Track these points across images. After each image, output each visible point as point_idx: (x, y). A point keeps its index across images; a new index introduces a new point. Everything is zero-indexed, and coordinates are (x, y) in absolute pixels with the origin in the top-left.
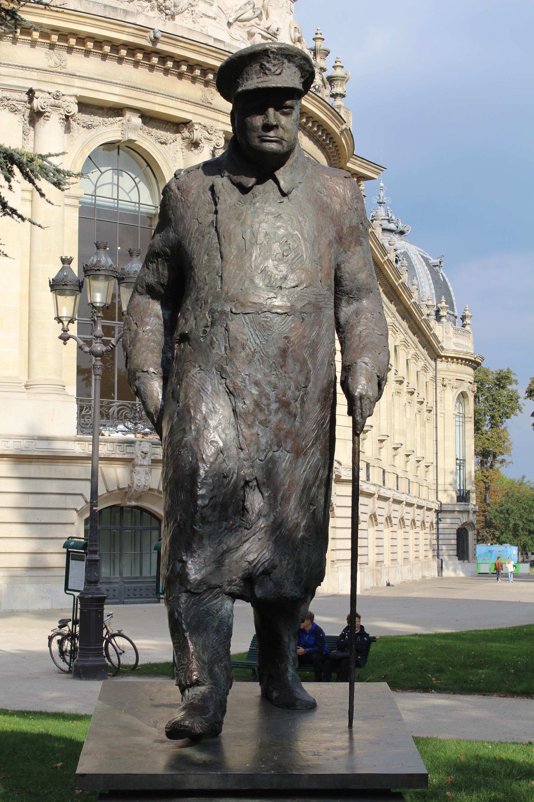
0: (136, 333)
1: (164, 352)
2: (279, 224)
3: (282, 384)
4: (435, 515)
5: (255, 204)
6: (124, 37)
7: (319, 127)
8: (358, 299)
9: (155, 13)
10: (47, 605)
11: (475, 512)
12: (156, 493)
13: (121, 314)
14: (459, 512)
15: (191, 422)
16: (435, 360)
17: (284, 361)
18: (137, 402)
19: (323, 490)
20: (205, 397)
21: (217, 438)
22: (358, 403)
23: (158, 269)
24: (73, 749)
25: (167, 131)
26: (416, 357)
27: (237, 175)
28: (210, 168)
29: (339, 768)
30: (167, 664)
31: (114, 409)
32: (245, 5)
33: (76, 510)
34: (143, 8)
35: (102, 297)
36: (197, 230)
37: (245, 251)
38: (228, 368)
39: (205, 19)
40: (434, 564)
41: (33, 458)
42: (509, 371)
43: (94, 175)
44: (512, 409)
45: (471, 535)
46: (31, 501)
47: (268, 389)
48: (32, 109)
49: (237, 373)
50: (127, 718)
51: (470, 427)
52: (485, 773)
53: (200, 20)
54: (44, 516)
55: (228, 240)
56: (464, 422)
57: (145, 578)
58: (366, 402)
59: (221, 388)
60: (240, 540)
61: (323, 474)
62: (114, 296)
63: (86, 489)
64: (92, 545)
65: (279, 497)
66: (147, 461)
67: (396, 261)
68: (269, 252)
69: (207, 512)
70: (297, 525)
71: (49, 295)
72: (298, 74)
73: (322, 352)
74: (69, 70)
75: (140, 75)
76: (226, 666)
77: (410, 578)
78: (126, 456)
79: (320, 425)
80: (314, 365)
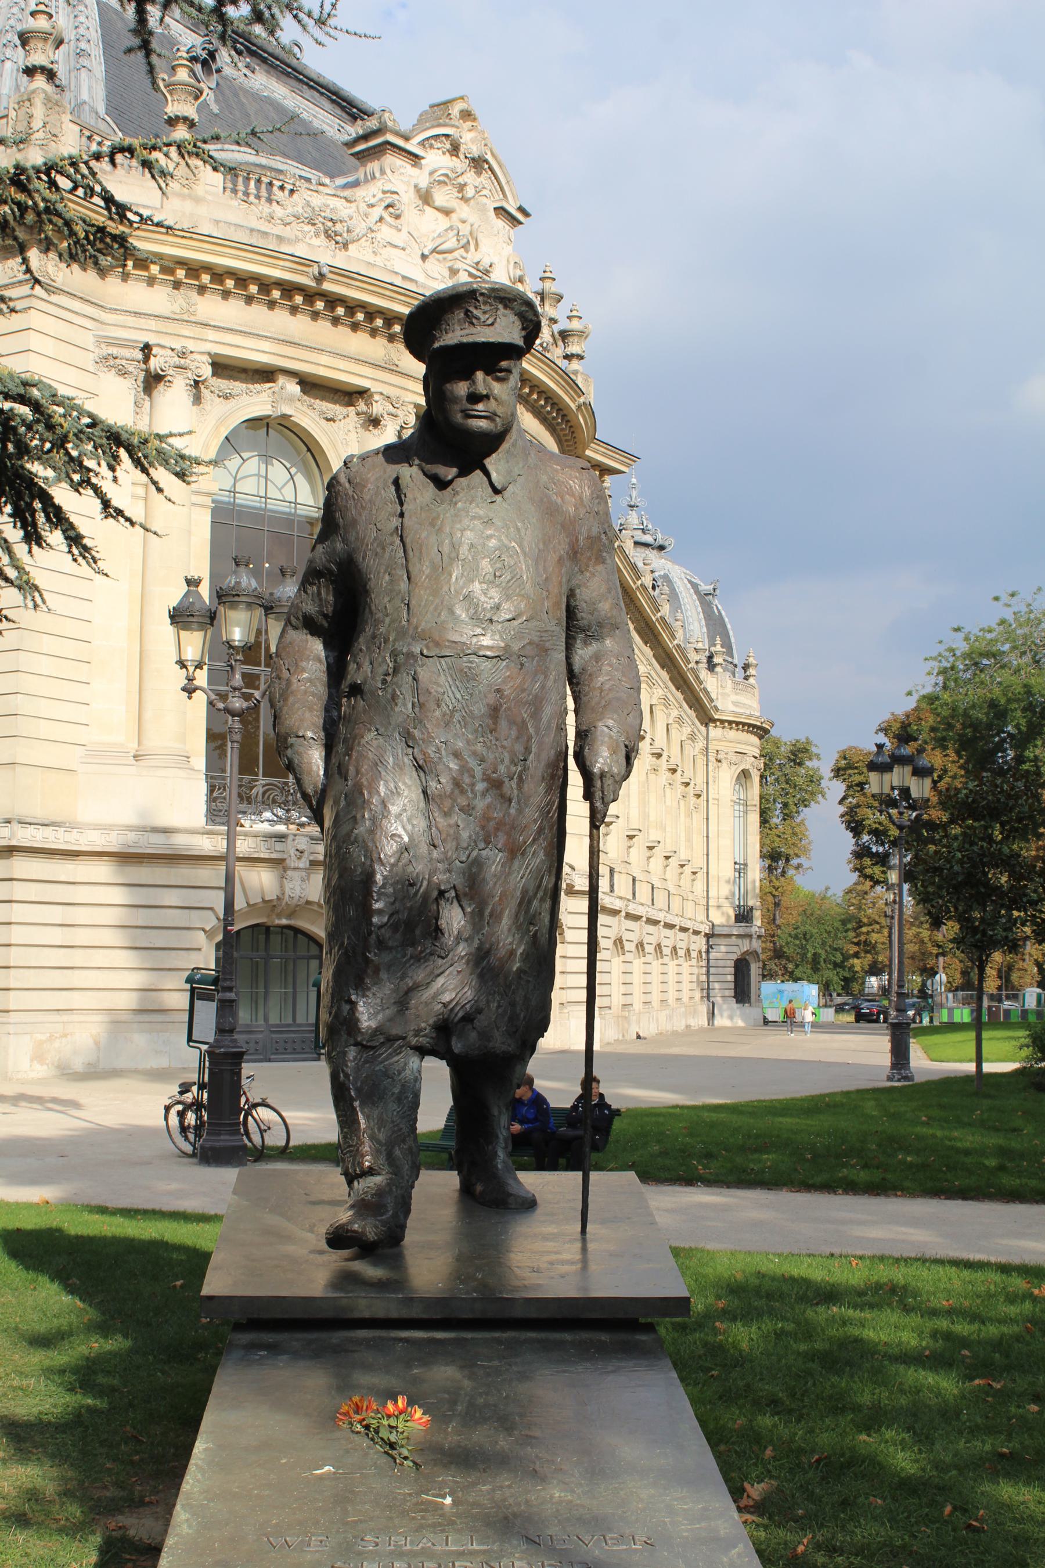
0: (289, 682)
1: (327, 710)
2: (489, 532)
4: (704, 940)
5: (456, 504)
6: (277, 274)
8: (599, 638)
11: (759, 937)
12: (315, 908)
13: (269, 656)
14: (739, 936)
15: (364, 808)
16: (706, 725)
19: (547, 905)
20: (383, 773)
22: (598, 784)
23: (319, 593)
25: (335, 403)
26: (680, 720)
28: (394, 453)
31: (258, 790)
32: (446, 230)
33: (203, 930)
35: (242, 634)
36: (375, 539)
37: (441, 569)
39: (389, 249)
40: (703, 1009)
41: (144, 858)
42: (808, 742)
44: (813, 794)
45: (755, 969)
46: (142, 917)
47: (472, 763)
48: (147, 371)
49: (429, 740)
50: (273, 1220)
51: (754, 818)
52: (769, 1296)
53: (384, 251)
55: (417, 554)
56: (746, 812)
57: (300, 1025)
58: (608, 781)
59: (406, 760)
60: (432, 972)
61: (548, 882)
62: (259, 632)
64: (225, 980)
65: (487, 913)
66: (303, 863)
67: (654, 588)
68: (475, 572)
69: (386, 933)
71: (169, 630)
72: (518, 324)
73: (548, 711)
74: (200, 317)
75: (299, 326)
76: (410, 1149)
77: (669, 1028)
78: (274, 856)
79: (545, 814)
80: (537, 729)
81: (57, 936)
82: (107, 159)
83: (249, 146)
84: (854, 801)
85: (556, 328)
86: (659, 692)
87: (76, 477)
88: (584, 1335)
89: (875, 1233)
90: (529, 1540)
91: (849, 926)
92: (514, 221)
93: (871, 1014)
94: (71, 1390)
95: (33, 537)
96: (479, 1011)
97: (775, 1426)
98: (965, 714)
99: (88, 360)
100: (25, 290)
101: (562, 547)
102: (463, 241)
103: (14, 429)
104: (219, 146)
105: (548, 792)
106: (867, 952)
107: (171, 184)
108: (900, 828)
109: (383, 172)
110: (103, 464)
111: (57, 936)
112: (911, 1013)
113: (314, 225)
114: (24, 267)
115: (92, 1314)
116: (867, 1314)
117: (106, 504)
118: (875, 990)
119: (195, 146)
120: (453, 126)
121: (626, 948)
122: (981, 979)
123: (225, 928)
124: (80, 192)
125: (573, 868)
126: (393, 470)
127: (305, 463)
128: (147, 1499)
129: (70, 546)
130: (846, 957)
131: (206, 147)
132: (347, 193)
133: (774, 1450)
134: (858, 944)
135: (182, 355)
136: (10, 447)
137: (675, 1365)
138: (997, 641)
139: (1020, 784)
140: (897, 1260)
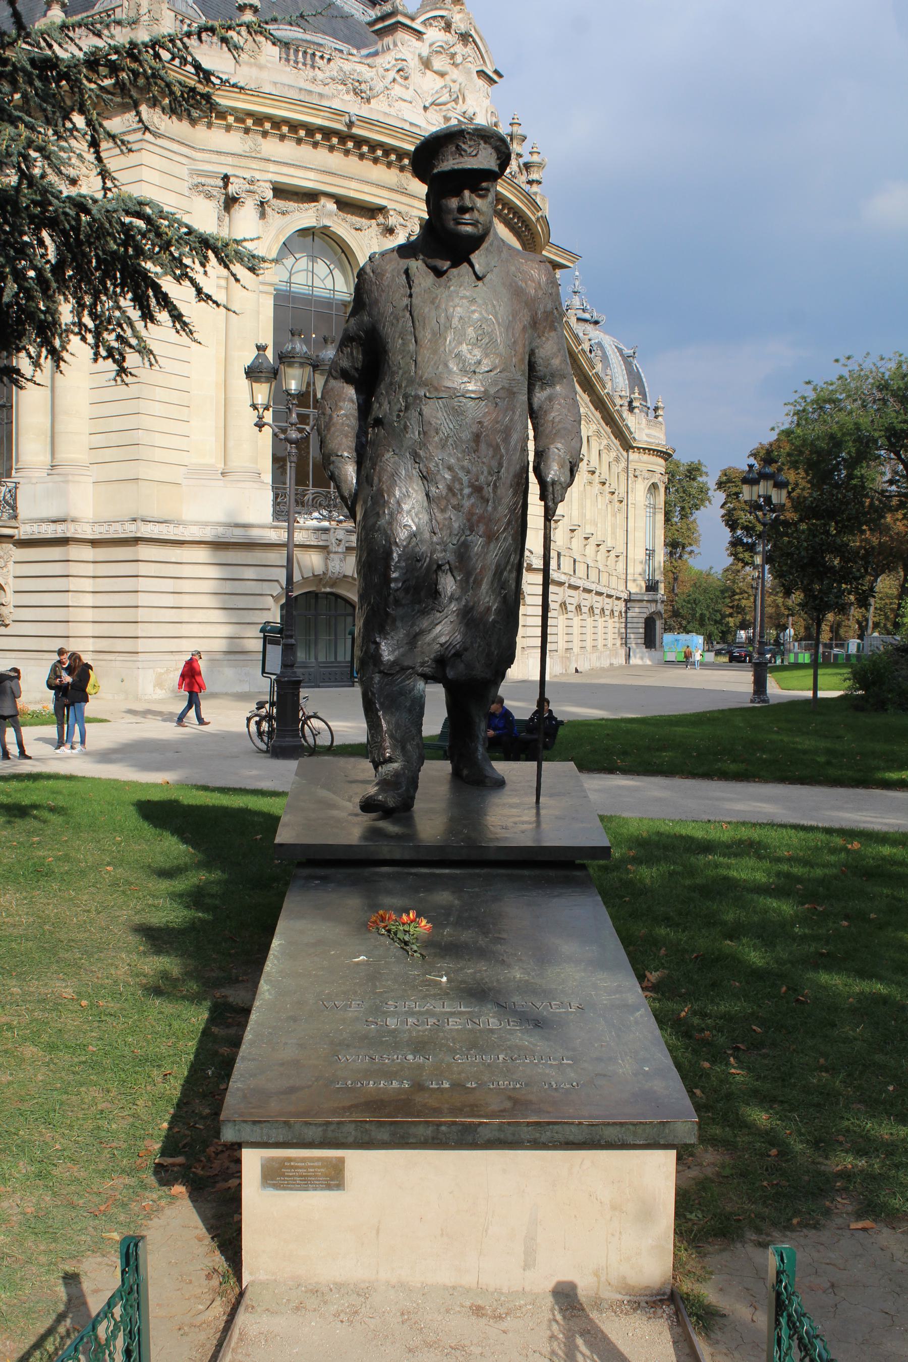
0: (331, 417)
1: (358, 437)
2: (473, 308)
3: (474, 469)
4: (624, 604)
6: (319, 121)
7: (515, 214)
8: (552, 385)
9: (350, 97)
10: (245, 688)
11: (663, 602)
12: (350, 580)
13: (316, 401)
14: (648, 601)
15: (384, 507)
16: (627, 451)
17: (477, 445)
18: (332, 490)
19: (514, 575)
20: (398, 482)
21: (410, 522)
22: (551, 489)
23: (352, 353)
24: (272, 822)
25: (362, 217)
26: (608, 447)
27: (432, 258)
28: (405, 251)
29: (527, 841)
30: (361, 745)
31: (309, 497)
32: (442, 88)
33: (272, 596)
34: (339, 91)
35: (297, 384)
36: (392, 313)
37: (439, 335)
38: (421, 453)
39: (400, 102)
40: (622, 652)
41: (230, 545)
42: (700, 463)
43: (289, 261)
44: (702, 500)
45: (659, 624)
46: (229, 587)
47: (461, 474)
48: (227, 195)
49: (430, 458)
50: (323, 793)
51: (660, 517)
52: (666, 848)
53: (396, 104)
54: (242, 602)
56: (654, 513)
57: (339, 662)
58: (558, 487)
59: (414, 472)
60: (433, 622)
61: (514, 559)
62: (308, 384)
63: (282, 575)
64: (287, 630)
65: (471, 580)
66: (341, 549)
67: (591, 351)
68: (464, 337)
69: (400, 594)
70: (489, 609)
71: (245, 382)
72: (494, 155)
73: (515, 437)
74: (264, 154)
75: (335, 160)
76: (418, 744)
77: (598, 665)
78: (321, 543)
79: (512, 511)
80: (507, 450)
81: (169, 600)
82: (195, 37)
83: (299, 26)
84: (732, 506)
85: (522, 161)
86: (594, 427)
87: (178, 272)
88: (537, 872)
89: (739, 806)
90: (499, 1005)
91: (726, 595)
92: (491, 81)
93: (740, 656)
94: (188, 907)
95: (148, 316)
96: (466, 649)
97: (668, 934)
98: (812, 444)
99: (184, 187)
100: (138, 136)
101: (526, 319)
102: (454, 96)
103: (133, 237)
104: (276, 27)
105: (514, 495)
106: (739, 613)
107: (242, 55)
108: (764, 525)
109: (395, 45)
110: (197, 261)
111: (169, 600)
112: (768, 656)
113: (346, 85)
114: (137, 118)
115: (200, 856)
116: (733, 861)
117: (199, 291)
118: (743, 640)
119: (259, 26)
120: (447, 9)
121: (569, 609)
122: (819, 633)
123: (287, 594)
124: (177, 62)
125: (531, 552)
126: (404, 263)
127: (340, 260)
128: (240, 978)
129: (174, 322)
130: (724, 616)
131: (268, 27)
132: (369, 61)
133: (666, 950)
134: (732, 607)
135: (251, 182)
136: (131, 251)
137: (600, 893)
138: (836, 391)
139: (850, 494)
140: (754, 825)
